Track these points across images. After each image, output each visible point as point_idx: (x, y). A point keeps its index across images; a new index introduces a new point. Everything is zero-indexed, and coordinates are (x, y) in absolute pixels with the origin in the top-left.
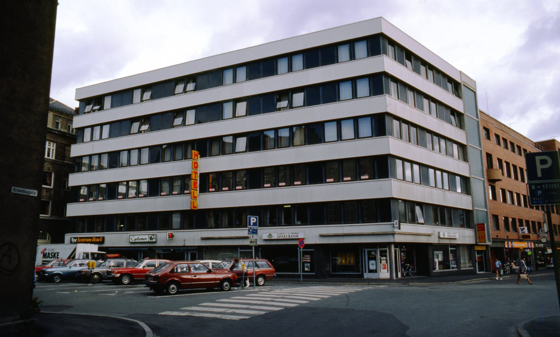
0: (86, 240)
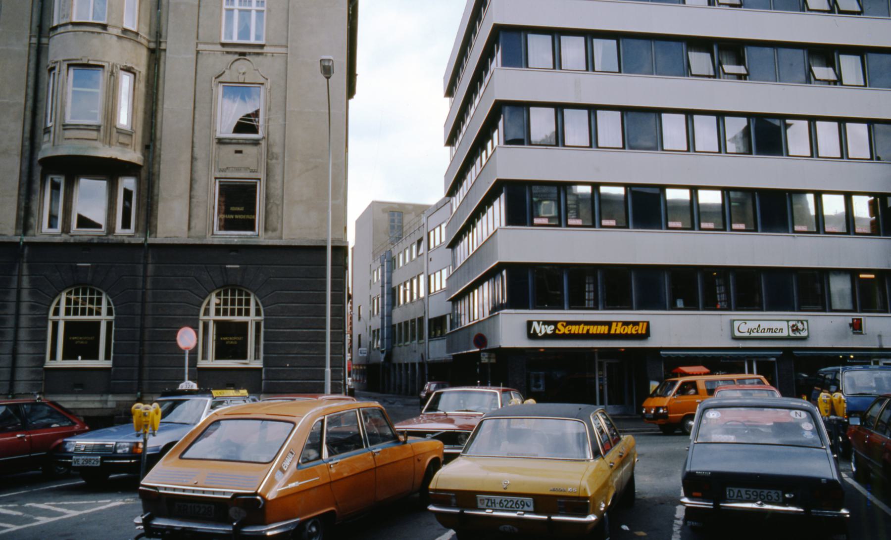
0: (588, 330)
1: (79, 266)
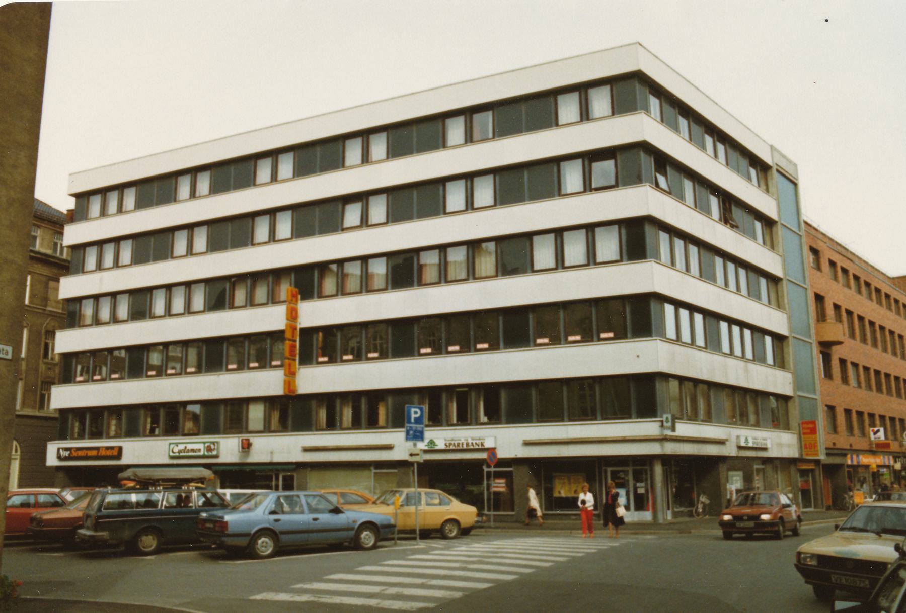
1: (313, 275)
